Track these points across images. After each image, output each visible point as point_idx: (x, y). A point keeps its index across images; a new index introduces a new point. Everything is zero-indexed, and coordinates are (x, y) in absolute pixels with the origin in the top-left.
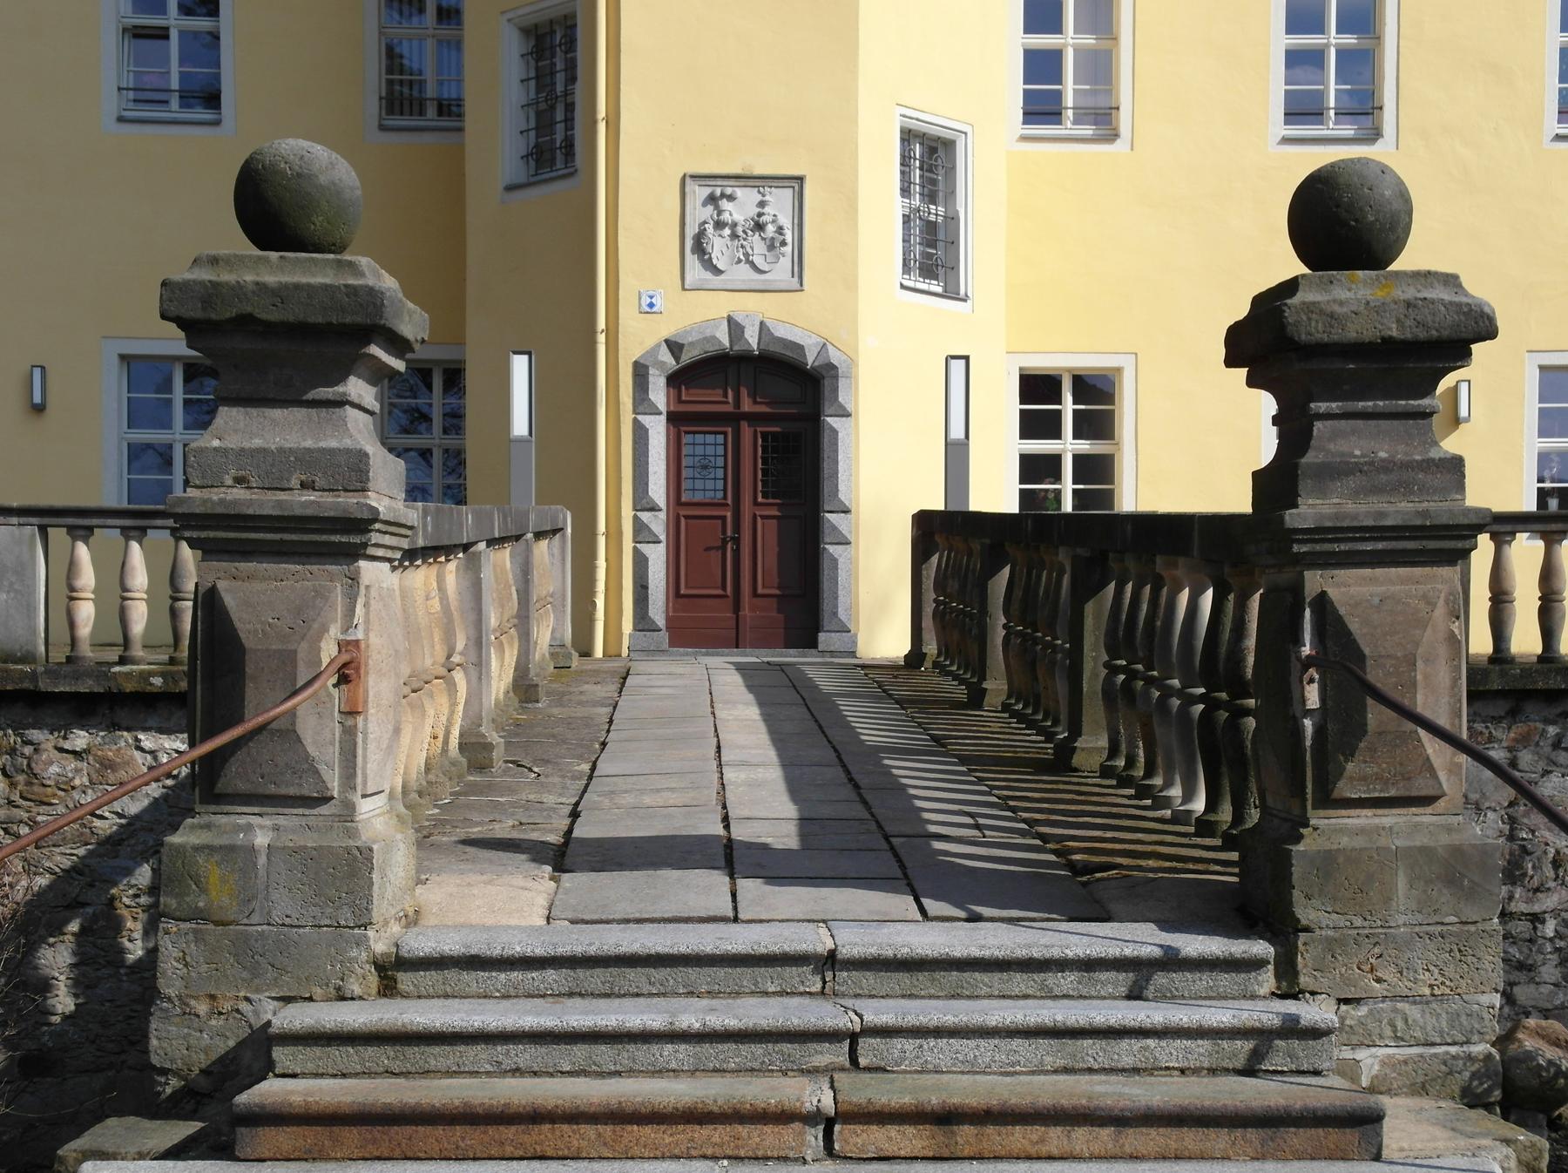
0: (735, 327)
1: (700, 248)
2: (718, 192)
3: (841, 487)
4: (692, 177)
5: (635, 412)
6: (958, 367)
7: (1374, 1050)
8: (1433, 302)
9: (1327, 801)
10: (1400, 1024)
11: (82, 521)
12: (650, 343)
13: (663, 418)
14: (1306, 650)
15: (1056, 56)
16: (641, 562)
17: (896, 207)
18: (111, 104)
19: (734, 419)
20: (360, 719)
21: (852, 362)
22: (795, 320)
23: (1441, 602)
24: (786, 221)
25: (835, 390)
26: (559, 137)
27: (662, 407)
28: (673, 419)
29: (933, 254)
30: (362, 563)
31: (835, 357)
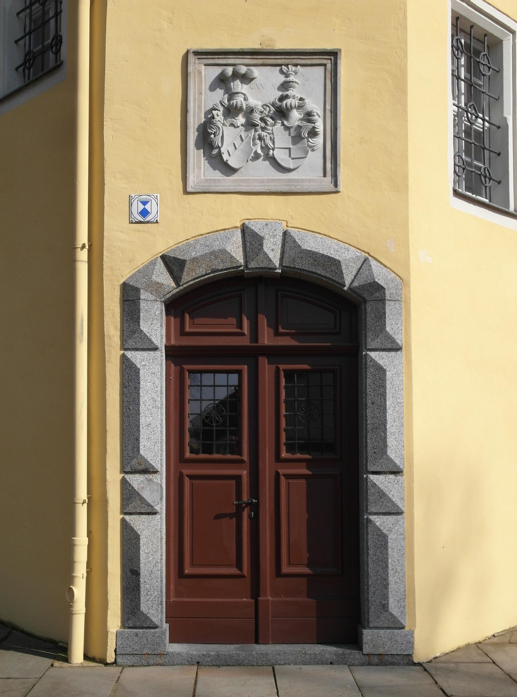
0: (250, 238)
1: (206, 140)
2: (230, 71)
3: (391, 441)
4: (197, 53)
5: (123, 347)
12: (142, 259)
13: (161, 356)
16: (130, 540)
19: (251, 354)
21: (403, 282)
22: (328, 228)
24: (315, 105)
25: (381, 317)
28: (173, 354)
31: (380, 275)
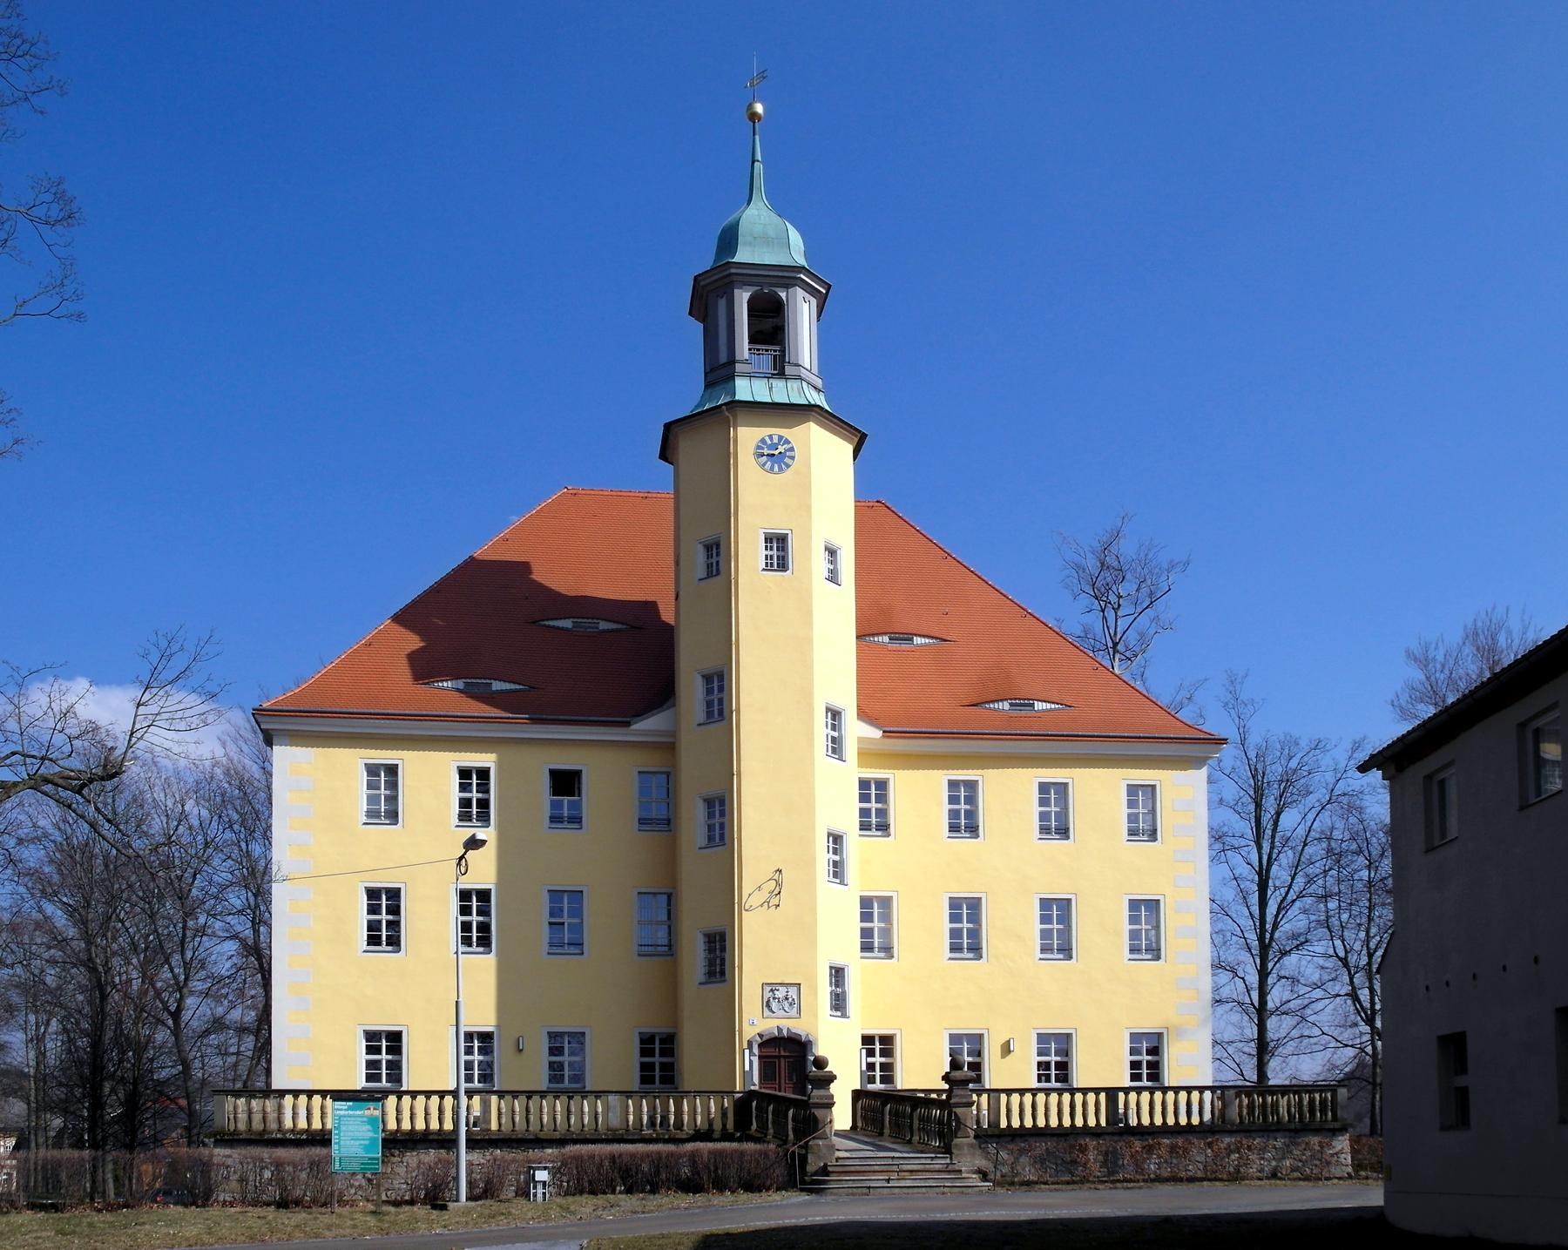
11: (543, 1094)
15: (872, 929)
17: (829, 989)
18: (546, 947)
19: (779, 1057)
22: (798, 1027)
29: (839, 1004)
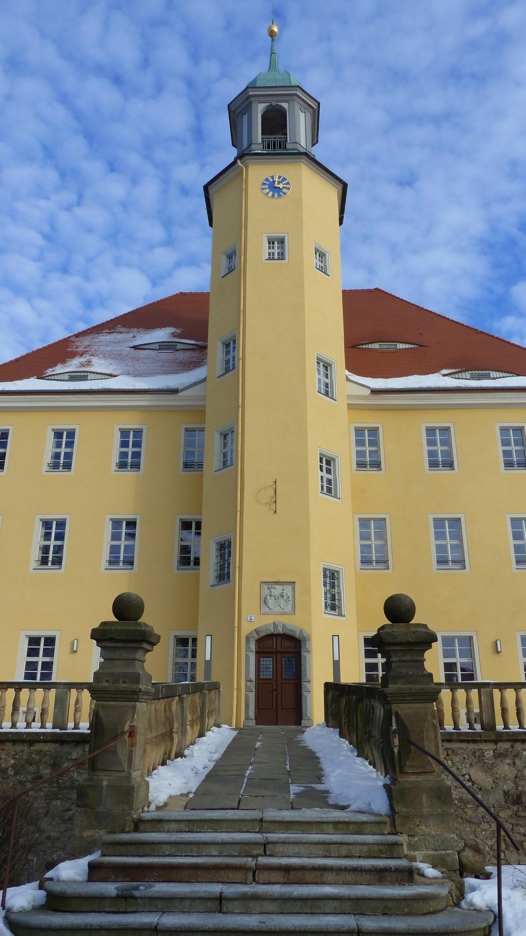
6: (336, 638)
7: (420, 852)
8: (420, 631)
9: (402, 772)
10: (427, 843)
14: (394, 727)
20: (134, 748)
22: (293, 623)
23: (430, 714)
24: (290, 594)
26: (226, 572)
27: (254, 650)
29: (333, 605)
30: (137, 703)
